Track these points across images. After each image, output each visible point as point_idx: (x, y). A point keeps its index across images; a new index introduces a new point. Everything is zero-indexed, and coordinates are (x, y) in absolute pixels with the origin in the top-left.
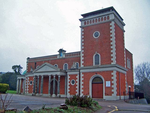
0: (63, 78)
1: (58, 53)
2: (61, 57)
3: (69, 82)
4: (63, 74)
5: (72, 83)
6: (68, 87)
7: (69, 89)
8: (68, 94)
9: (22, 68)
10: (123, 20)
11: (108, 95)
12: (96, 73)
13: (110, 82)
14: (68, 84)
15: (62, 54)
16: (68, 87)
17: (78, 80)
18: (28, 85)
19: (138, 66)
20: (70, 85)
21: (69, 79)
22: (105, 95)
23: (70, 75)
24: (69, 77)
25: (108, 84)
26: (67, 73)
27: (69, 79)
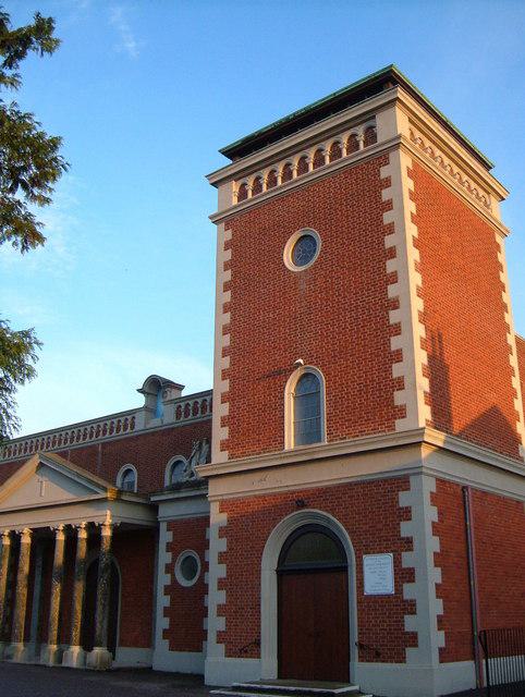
1: (139, 401)
2: (155, 423)
3: (169, 569)
4: (136, 516)
5: (182, 569)
6: (163, 601)
8: (161, 644)
10: (488, 167)
11: (378, 654)
12: (300, 500)
13: (388, 559)
14: (163, 580)
15: (162, 408)
18: (166, 588)
19: (19, 76)
21: (170, 547)
22: (362, 659)
23: (172, 525)
24: (166, 536)
25: (377, 574)
26: (153, 508)
27: (170, 547)
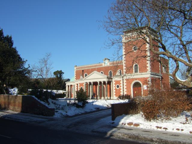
0: (109, 83)
3: (115, 87)
7: (115, 92)
9: (64, 73)
12: (136, 79)
14: (114, 88)
16: (114, 91)
17: (121, 85)
20: (116, 89)
21: (115, 84)
24: (114, 83)
27: (115, 84)
